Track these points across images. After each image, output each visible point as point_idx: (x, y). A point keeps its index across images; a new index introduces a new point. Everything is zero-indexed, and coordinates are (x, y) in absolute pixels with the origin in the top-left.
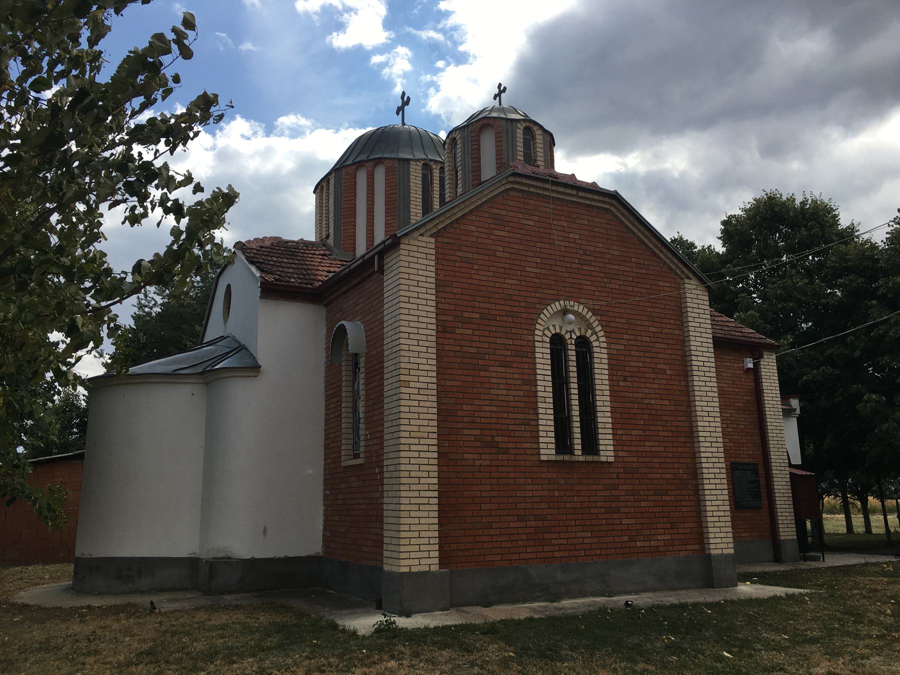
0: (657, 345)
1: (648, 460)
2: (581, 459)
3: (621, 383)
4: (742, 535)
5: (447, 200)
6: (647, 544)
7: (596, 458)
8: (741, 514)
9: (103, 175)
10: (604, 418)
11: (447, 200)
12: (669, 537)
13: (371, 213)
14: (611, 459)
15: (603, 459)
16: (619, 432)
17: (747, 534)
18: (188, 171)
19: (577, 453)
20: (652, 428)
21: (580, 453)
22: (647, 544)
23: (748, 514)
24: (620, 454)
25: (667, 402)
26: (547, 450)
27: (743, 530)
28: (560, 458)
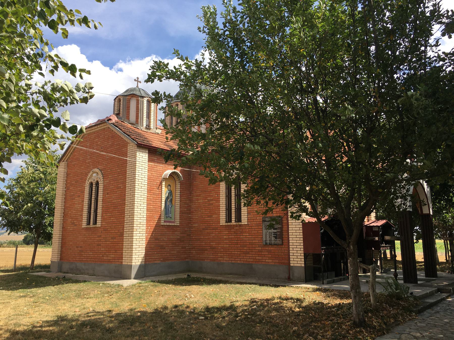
0: (119, 177)
1: (111, 225)
2: (235, 224)
3: (107, 196)
4: (267, 261)
5: (41, 140)
6: (107, 258)
7: (240, 223)
8: (267, 248)
9: (45, 128)
10: (99, 211)
11: (41, 140)
12: (114, 256)
13: (128, 114)
14: (178, 225)
15: (243, 223)
16: (104, 215)
17: (271, 261)
18: (145, 82)
19: (232, 222)
20: (114, 212)
21: (234, 222)
22: (107, 258)
23: (272, 248)
24: (103, 223)
25: (120, 200)
26: (223, 221)
27: (268, 258)
28: (227, 224)
